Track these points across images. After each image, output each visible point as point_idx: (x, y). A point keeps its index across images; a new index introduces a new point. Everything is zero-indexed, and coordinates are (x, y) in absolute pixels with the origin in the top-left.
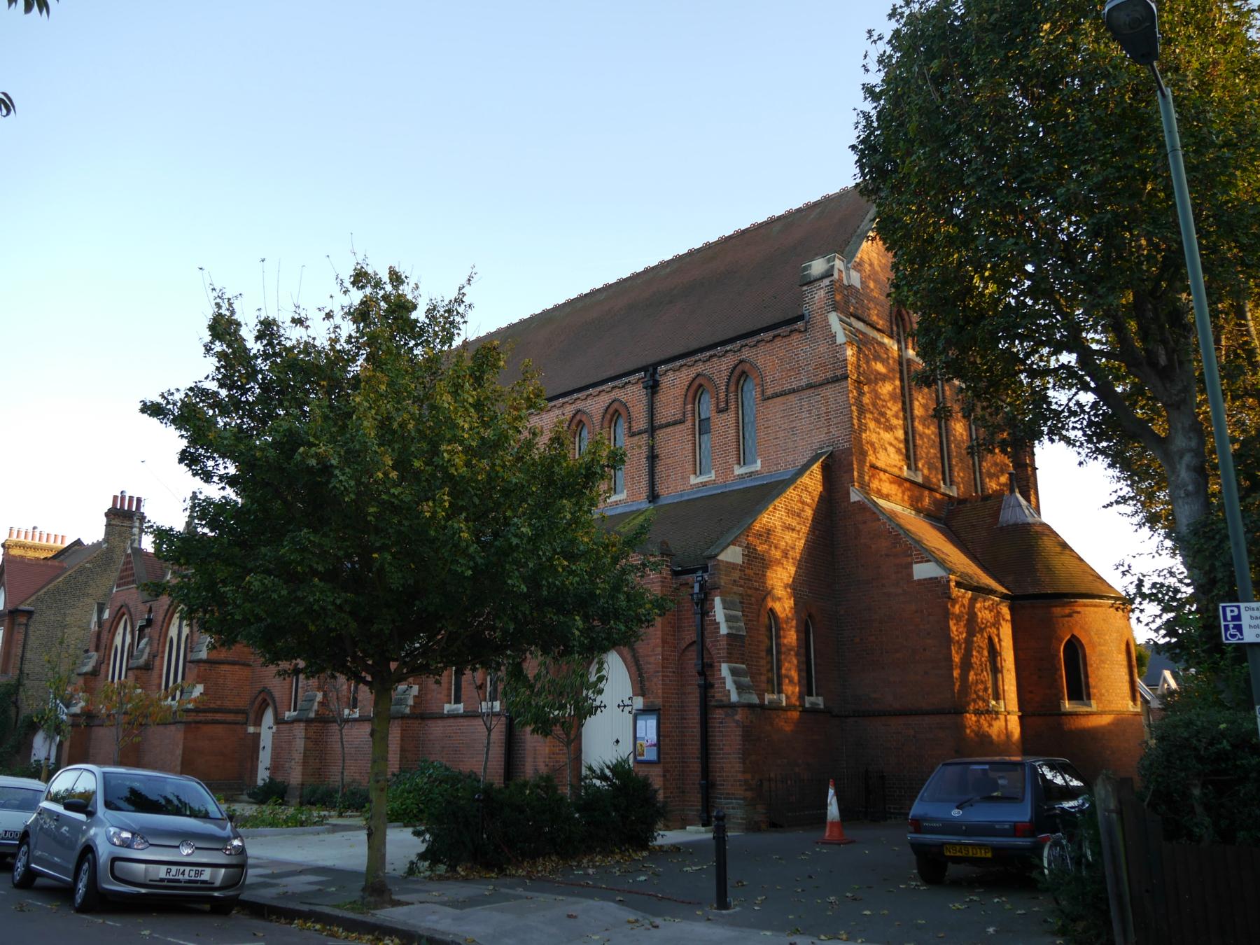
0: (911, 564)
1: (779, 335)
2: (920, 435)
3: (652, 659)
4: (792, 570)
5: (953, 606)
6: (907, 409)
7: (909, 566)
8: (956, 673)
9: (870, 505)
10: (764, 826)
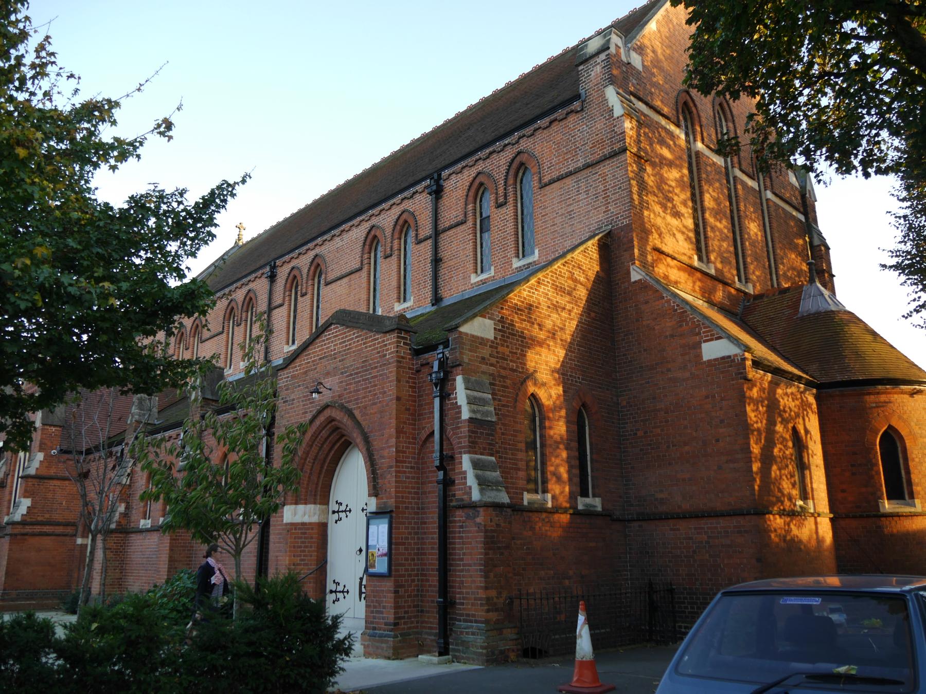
0: (700, 343)
1: (555, 120)
2: (712, 228)
3: (386, 453)
4: (562, 353)
5: (751, 389)
6: (696, 198)
7: (698, 346)
8: (755, 467)
9: (652, 282)
10: (512, 656)
